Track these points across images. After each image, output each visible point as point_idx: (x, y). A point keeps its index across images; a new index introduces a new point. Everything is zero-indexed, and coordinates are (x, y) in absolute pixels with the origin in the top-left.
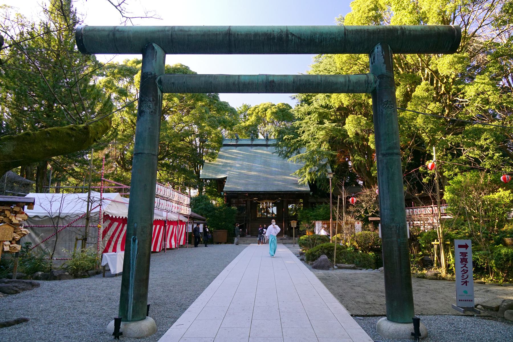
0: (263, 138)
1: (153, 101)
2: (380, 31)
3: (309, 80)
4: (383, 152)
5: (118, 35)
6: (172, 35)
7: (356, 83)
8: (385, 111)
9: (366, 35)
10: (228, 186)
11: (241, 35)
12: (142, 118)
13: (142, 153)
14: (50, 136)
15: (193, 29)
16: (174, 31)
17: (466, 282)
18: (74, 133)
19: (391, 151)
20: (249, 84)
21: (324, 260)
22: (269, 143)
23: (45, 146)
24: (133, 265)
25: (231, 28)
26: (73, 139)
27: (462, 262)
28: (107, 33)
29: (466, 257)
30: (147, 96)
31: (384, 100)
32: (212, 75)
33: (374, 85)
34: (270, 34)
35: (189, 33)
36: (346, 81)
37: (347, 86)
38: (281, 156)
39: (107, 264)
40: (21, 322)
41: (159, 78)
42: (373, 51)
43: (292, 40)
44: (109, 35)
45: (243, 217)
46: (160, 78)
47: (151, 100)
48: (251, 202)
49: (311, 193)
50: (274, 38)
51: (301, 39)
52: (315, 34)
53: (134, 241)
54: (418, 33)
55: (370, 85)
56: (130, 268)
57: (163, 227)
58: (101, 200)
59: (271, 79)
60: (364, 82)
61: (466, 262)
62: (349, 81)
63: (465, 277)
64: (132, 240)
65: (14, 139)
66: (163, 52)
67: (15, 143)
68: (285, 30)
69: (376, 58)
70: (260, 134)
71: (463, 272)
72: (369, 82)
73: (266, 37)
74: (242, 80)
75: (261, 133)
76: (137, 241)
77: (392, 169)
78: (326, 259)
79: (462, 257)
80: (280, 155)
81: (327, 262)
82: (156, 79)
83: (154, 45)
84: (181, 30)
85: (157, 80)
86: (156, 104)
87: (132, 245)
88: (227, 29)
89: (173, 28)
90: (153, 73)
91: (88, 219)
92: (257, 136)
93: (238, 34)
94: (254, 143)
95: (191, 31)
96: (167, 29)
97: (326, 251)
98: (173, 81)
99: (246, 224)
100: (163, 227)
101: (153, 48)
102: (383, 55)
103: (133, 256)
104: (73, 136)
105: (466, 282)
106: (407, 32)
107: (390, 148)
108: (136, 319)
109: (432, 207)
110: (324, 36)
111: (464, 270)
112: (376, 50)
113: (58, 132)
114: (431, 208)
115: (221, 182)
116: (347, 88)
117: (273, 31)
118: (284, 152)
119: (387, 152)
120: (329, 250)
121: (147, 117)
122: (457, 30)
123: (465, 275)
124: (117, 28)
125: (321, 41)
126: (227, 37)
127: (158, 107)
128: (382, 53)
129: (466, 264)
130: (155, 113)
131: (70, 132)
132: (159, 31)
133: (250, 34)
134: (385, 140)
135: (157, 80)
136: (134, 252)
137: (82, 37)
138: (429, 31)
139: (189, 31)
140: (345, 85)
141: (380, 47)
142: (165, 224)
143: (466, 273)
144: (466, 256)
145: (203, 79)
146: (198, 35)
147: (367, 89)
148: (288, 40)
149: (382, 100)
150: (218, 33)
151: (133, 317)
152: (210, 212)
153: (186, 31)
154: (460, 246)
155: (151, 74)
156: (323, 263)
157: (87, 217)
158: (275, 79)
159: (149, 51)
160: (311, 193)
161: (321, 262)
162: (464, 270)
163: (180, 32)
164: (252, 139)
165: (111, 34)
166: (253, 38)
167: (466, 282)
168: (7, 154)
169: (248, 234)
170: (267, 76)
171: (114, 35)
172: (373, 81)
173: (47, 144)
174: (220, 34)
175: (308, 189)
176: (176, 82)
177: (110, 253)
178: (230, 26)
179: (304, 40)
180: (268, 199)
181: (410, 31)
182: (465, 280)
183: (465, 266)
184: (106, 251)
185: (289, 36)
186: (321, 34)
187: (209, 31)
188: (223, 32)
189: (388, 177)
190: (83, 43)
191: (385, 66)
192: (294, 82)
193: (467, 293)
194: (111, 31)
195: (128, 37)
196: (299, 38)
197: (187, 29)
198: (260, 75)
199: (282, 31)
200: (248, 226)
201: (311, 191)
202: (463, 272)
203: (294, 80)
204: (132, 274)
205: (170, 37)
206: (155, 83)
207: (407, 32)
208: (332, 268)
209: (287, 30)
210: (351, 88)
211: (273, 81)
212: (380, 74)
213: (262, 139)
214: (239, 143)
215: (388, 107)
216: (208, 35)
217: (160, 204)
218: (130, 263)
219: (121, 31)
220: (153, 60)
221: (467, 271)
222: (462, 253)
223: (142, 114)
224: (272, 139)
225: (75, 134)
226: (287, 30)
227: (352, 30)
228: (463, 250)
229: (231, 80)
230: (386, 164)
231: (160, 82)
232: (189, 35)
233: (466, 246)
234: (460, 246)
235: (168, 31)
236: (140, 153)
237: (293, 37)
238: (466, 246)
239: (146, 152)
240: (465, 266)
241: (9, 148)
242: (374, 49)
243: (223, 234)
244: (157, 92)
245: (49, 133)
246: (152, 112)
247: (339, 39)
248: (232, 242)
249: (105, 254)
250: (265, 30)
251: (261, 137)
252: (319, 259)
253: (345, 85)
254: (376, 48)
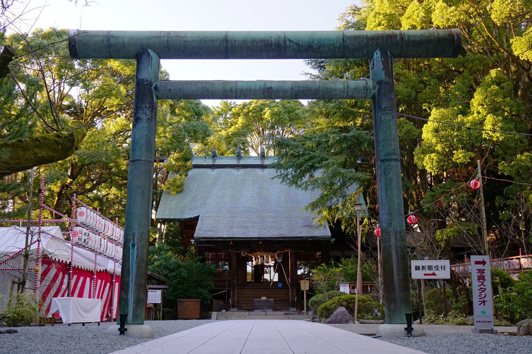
0: (255, 155)
1: (150, 107)
2: (379, 37)
3: (307, 86)
4: (381, 158)
5: (112, 41)
6: (167, 41)
7: (355, 89)
8: (383, 118)
9: (365, 41)
10: (202, 231)
11: (238, 41)
12: (139, 125)
13: (139, 160)
14: (40, 143)
15: (189, 35)
16: (170, 37)
17: (484, 302)
18: (60, 140)
19: (389, 157)
20: (246, 90)
21: (341, 313)
22: (267, 162)
23: (36, 154)
24: (132, 270)
25: (228, 34)
26: (60, 147)
27: (479, 279)
28: (101, 39)
29: (484, 274)
30: (143, 103)
31: (383, 107)
32: (209, 81)
33: (373, 92)
34: (268, 41)
35: (186, 39)
36: (344, 88)
37: (346, 91)
38: (284, 183)
39: (58, 311)
40: (13, 333)
41: (154, 84)
42: (372, 57)
43: (290, 47)
44: (103, 41)
45: (225, 281)
46: (156, 85)
47: (148, 107)
48: (239, 255)
49: (333, 240)
50: (271, 45)
51: (299, 45)
52: (313, 40)
53: (133, 246)
54: (417, 39)
55: (369, 91)
56: (129, 272)
57: (108, 284)
58: (39, 233)
59: (268, 85)
60: (362, 88)
61: (484, 280)
62: (348, 87)
63: (483, 296)
64: (131, 245)
65: (9, 145)
66: (158, 57)
67: (10, 149)
68: (283, 36)
69: (375, 63)
70: (251, 150)
71: (480, 291)
72: (368, 88)
73: (264, 44)
74: (240, 86)
75: (252, 147)
76: (136, 246)
77: (390, 174)
78: (344, 312)
79: (479, 274)
80: (283, 180)
81: (345, 315)
82: (152, 85)
83: (149, 51)
84: (177, 36)
85: (153, 86)
86: (152, 111)
87: (131, 251)
88: (224, 35)
89: (169, 33)
90: (149, 79)
91: (26, 256)
92: (247, 152)
93: (235, 41)
94: (242, 162)
95: (187, 37)
96: (162, 35)
97: (345, 303)
98: (169, 87)
99: (229, 291)
100: (108, 284)
101: (149, 54)
102: (382, 61)
103: (133, 261)
104: (60, 143)
105: (484, 302)
106: (406, 38)
107: (388, 154)
108: (136, 323)
109: (519, 259)
110: (323, 42)
111: (481, 288)
112: (375, 56)
113: (46, 139)
114: (518, 261)
115: (190, 224)
116: (346, 94)
117: (271, 37)
118: (289, 176)
119: (386, 158)
120: (349, 303)
121: (143, 124)
122: (457, 34)
123: (483, 294)
124: (111, 34)
125: (320, 47)
126: (224, 43)
127: (154, 114)
128: (381, 58)
129: (483, 282)
130: (152, 120)
131: (56, 139)
132: (154, 37)
133: (248, 41)
134: (383, 146)
135: (153, 86)
136: (133, 257)
137: (75, 42)
138: (428, 37)
139: (185, 37)
140: (344, 92)
141: (379, 52)
142: (112, 279)
143: (483, 291)
144: (483, 273)
145: (200, 85)
146: (194, 41)
147: (366, 96)
148: (285, 47)
149: (381, 107)
150: (215, 39)
151: (133, 320)
152: (173, 271)
153: (183, 37)
154: (477, 263)
155: (147, 80)
156: (340, 317)
157: (26, 255)
158: (273, 86)
159: (144, 58)
160: (333, 240)
161: (337, 315)
162: (481, 288)
163: (176, 39)
164: (239, 157)
165: (105, 39)
166: (250, 45)
167: (484, 302)
168: (5, 160)
169: (233, 307)
170: (265, 82)
171: (108, 40)
172: (371, 87)
173: (37, 151)
174: (217, 40)
175: (327, 233)
176: (173, 89)
177: (59, 297)
178: (227, 32)
179: (302, 46)
180: (265, 251)
181: (409, 36)
182: (482, 300)
183: (482, 284)
184: (56, 295)
185: (287, 42)
186: (319, 40)
187: (206, 37)
188: (220, 39)
189: (386, 183)
190: (75, 49)
191: (384, 72)
192: (292, 89)
193: (485, 313)
194: (105, 37)
195: (123, 43)
196: (297, 44)
197: (183, 35)
198: (258, 81)
199: (279, 38)
200: (234, 294)
201: (332, 237)
202: (480, 291)
203: (292, 86)
204: (132, 278)
205: (166, 43)
206: (151, 90)
207: (406, 38)
208: (352, 322)
209: (285, 37)
210: (350, 94)
211: (271, 88)
212: (379, 80)
213: (254, 157)
214: (218, 162)
215: (387, 113)
216: (205, 41)
217: (107, 248)
218: (129, 268)
219: (116, 37)
220: (149, 66)
221: (485, 289)
222: (479, 270)
223: (139, 121)
224: (271, 157)
225: (61, 142)
226: (285, 37)
227: (351, 36)
228: (480, 267)
229: (228, 87)
230: (384, 170)
231: (156, 88)
232: (186, 41)
233: (484, 263)
234: (477, 263)
235: (164, 37)
236: (137, 160)
237: (291, 44)
238: (484, 263)
239: (143, 159)
240: (482, 284)
241: (6, 154)
242: (373, 55)
243: (193, 305)
244: (153, 99)
245: (39, 140)
246: (148, 119)
247: (338, 45)
248: (209, 317)
249: (54, 299)
250: (262, 36)
251: (253, 154)
252: (335, 313)
253: (344, 92)
254: (375, 53)
